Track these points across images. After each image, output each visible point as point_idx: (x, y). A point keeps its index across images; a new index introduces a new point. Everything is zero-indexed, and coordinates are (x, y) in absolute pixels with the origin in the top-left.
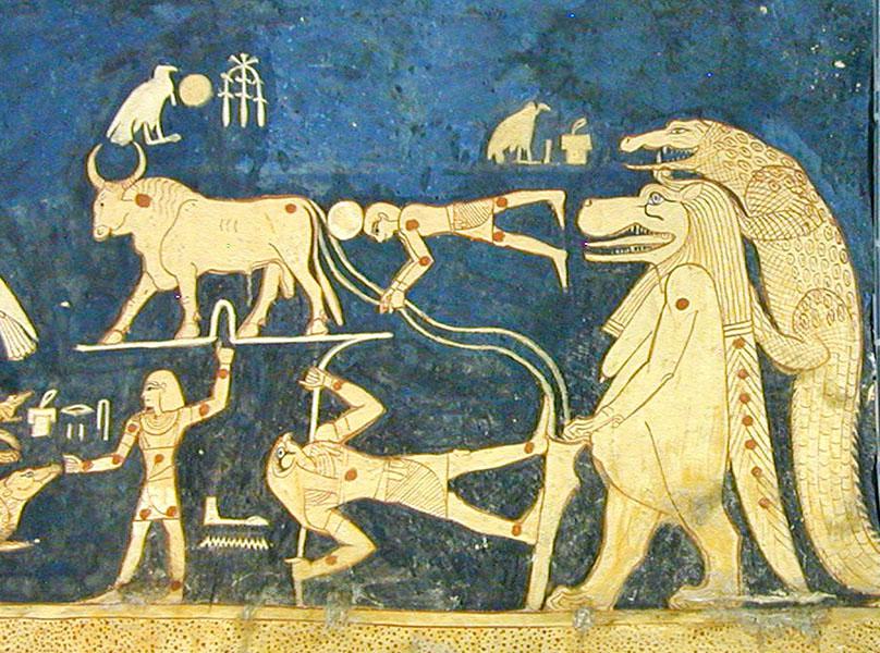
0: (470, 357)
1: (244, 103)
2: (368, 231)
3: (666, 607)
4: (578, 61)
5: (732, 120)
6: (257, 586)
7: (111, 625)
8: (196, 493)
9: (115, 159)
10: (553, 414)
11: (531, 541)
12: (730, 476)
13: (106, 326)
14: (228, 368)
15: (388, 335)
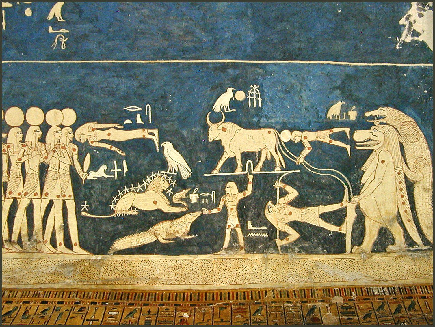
0: (324, 178)
1: (250, 99)
2: (293, 139)
3: (386, 251)
4: (353, 89)
5: (396, 107)
6: (267, 248)
7: (224, 261)
8: (244, 220)
9: (214, 116)
10: (348, 195)
11: (345, 233)
12: (399, 213)
13: (214, 169)
14: (251, 181)
15: (299, 171)
